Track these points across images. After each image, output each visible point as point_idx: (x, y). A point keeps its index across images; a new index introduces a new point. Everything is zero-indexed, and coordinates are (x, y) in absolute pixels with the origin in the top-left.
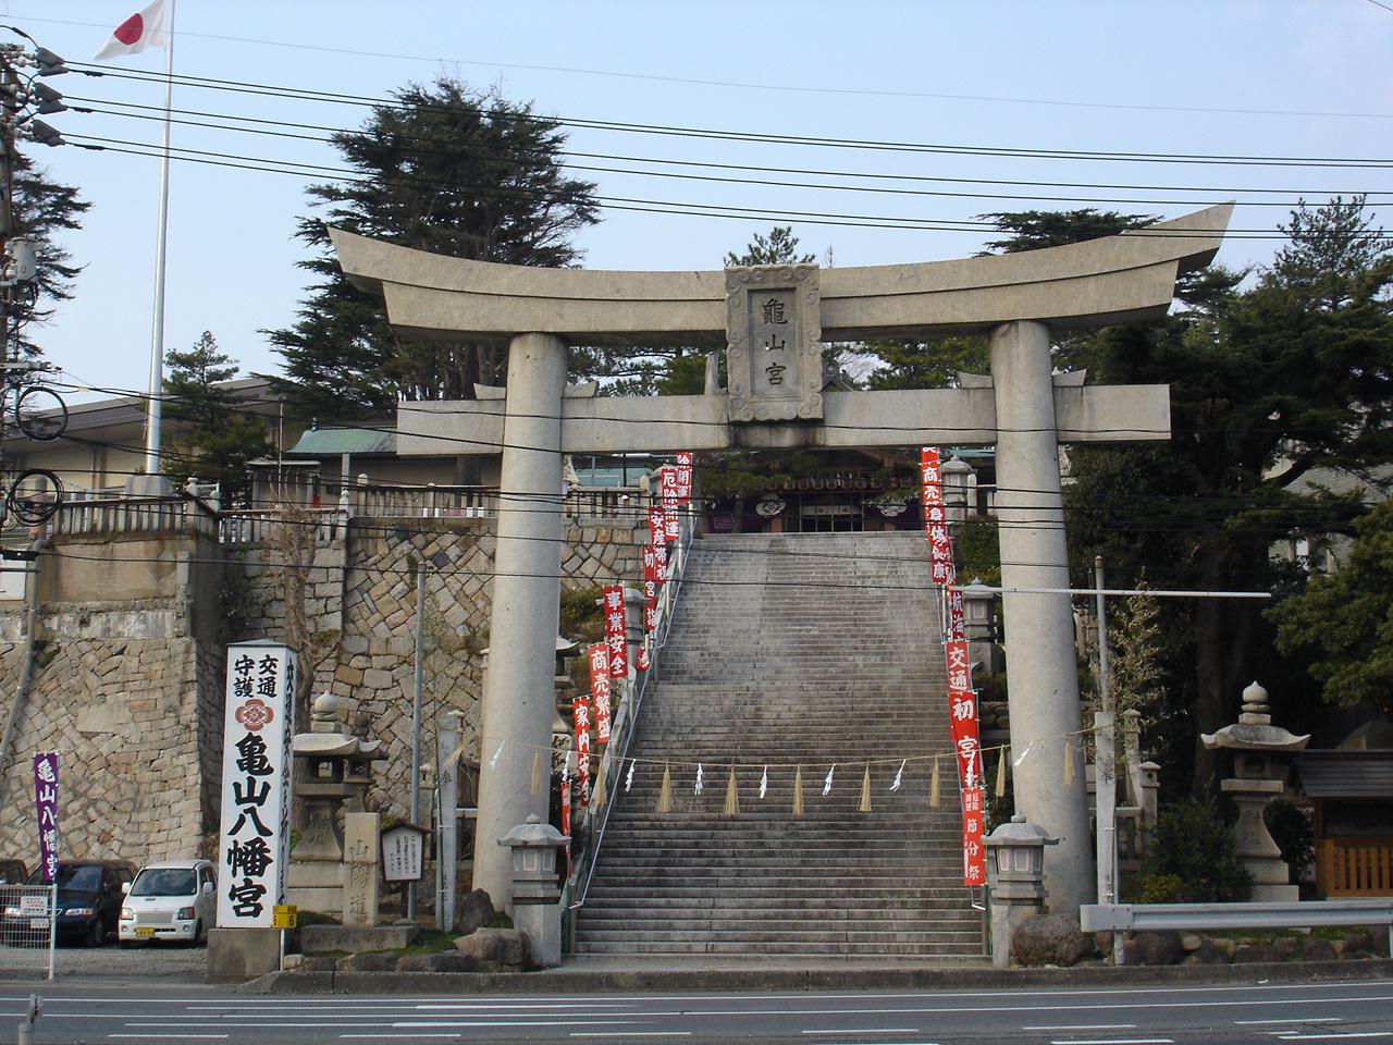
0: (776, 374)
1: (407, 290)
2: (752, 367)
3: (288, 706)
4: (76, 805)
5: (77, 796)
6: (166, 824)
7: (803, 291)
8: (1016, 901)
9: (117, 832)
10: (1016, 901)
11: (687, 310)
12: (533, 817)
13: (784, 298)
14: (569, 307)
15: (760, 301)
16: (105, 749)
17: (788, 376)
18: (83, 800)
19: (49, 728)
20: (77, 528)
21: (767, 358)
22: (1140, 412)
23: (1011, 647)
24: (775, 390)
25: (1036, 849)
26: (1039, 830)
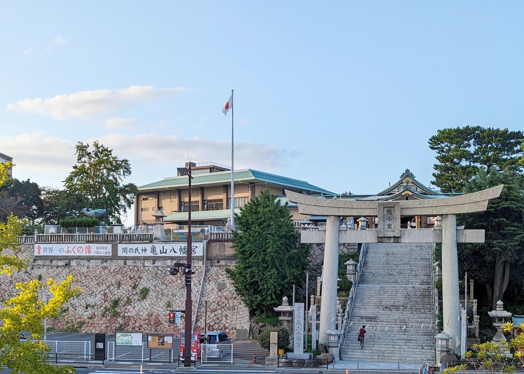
0: (389, 226)
1: (303, 205)
2: (384, 224)
3: (304, 343)
4: (219, 308)
5: (219, 305)
6: (240, 313)
7: (396, 208)
8: (442, 351)
9: (229, 315)
10: (442, 351)
11: (368, 211)
12: (332, 328)
13: (392, 209)
14: (341, 210)
15: (386, 209)
16: (225, 294)
17: (393, 227)
18: (220, 307)
19: (211, 288)
20: (212, 238)
21: (388, 222)
22: (476, 236)
23: (443, 277)
24: (389, 230)
25: (447, 340)
26: (448, 335)
